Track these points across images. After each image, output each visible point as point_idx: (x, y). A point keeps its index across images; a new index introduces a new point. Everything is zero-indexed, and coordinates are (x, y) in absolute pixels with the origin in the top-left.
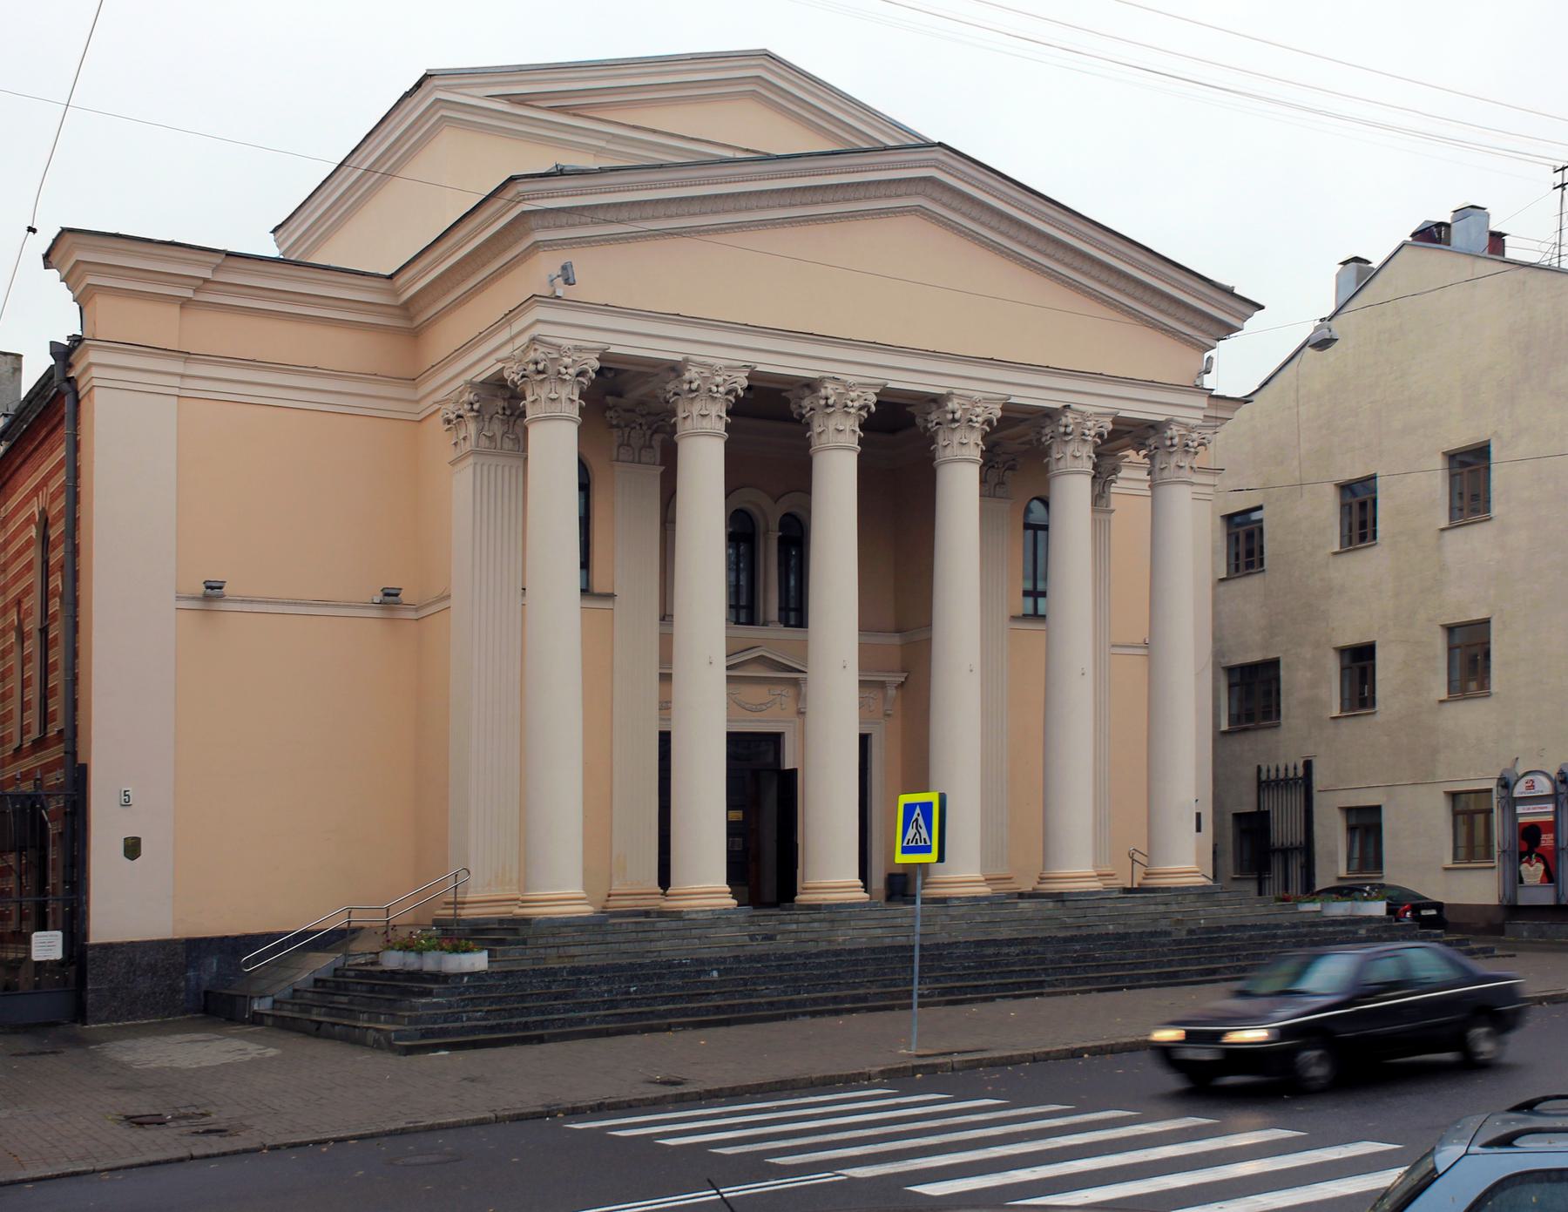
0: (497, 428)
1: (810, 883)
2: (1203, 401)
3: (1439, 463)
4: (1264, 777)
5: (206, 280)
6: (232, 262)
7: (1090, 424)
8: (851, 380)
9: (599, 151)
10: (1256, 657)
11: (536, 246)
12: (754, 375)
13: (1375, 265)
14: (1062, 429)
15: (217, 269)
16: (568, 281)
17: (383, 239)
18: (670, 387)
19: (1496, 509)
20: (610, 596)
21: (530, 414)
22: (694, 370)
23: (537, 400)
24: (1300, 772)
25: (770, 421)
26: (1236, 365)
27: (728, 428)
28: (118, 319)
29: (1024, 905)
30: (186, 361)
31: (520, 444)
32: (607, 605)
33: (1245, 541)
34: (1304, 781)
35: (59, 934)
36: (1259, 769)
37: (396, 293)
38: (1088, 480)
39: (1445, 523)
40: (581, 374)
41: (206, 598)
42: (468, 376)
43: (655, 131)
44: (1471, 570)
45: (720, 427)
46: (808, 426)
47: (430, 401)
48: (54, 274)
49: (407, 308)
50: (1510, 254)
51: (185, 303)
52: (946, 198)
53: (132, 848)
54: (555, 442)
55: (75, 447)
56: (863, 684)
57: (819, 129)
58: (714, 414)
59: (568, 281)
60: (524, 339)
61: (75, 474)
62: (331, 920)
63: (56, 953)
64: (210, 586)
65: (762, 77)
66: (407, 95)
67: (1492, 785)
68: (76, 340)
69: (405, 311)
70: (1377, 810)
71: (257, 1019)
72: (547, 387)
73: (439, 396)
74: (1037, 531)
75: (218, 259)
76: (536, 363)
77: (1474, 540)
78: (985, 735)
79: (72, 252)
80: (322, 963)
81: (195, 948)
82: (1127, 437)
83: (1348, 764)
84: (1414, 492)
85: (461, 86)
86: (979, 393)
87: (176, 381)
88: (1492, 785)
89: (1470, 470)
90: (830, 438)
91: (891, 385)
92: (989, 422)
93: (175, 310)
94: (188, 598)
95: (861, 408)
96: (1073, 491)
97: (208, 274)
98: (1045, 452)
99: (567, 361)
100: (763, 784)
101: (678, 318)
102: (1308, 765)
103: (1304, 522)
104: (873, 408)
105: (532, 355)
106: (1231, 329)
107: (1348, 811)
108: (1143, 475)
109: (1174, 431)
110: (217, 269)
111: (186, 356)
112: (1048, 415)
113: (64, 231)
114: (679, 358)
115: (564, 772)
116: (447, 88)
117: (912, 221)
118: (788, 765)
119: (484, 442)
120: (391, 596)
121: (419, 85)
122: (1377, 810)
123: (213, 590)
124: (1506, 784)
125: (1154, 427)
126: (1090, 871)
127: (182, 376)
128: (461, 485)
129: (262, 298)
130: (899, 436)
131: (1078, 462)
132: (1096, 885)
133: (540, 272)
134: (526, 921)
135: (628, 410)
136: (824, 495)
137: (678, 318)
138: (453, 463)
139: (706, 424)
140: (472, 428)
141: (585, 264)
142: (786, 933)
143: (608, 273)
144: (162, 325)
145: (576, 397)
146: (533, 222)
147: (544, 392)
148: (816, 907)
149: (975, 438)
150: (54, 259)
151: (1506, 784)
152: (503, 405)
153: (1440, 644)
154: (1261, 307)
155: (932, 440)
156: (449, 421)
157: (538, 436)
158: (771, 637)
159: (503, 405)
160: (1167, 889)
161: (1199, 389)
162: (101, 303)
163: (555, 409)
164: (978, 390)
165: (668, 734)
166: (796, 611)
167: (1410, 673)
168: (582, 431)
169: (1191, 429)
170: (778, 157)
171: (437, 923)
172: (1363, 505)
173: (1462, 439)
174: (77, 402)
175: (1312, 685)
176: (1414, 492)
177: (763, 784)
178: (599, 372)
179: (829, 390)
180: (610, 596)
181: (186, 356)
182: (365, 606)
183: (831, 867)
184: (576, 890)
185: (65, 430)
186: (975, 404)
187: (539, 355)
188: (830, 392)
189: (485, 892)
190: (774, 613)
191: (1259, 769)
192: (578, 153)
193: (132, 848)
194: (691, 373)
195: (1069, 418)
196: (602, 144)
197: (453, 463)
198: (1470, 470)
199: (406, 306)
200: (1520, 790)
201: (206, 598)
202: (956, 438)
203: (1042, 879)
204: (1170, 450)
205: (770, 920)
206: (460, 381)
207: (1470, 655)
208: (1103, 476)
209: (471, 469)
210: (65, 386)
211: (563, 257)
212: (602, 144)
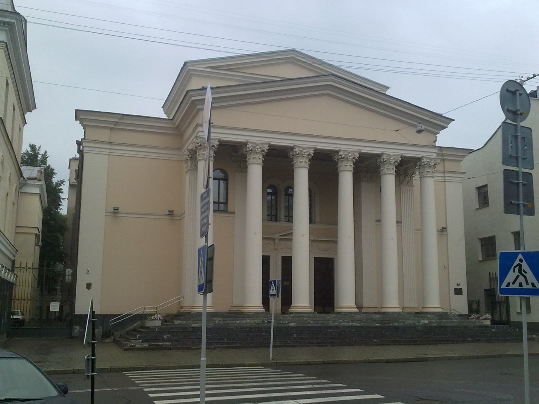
1: (340, 305)
2: (436, 151)
4: (491, 276)
5: (117, 122)
8: (304, 146)
14: (382, 160)
15: (120, 119)
22: (250, 144)
25: (278, 161)
32: (231, 215)
36: (490, 273)
41: (114, 212)
49: (177, 127)
51: (111, 129)
53: (89, 286)
56: (264, 238)
57: (311, 70)
58: (257, 157)
65: (292, 57)
72: (202, 151)
75: (120, 116)
76: (198, 143)
79: (80, 115)
86: (349, 149)
87: (108, 151)
91: (318, 147)
94: (109, 213)
95: (308, 155)
97: (117, 120)
101: (245, 129)
104: (313, 155)
109: (424, 160)
110: (120, 119)
114: (245, 141)
116: (193, 66)
120: (171, 212)
127: (110, 149)
129: (145, 128)
130: (324, 165)
135: (230, 158)
136: (307, 182)
137: (245, 129)
142: (329, 319)
144: (104, 135)
147: (201, 152)
148: (339, 313)
152: (193, 156)
154: (454, 120)
158: (282, 224)
161: (434, 147)
166: (289, 218)
170: (292, 79)
180: (234, 213)
183: (346, 300)
187: (198, 141)
191: (490, 273)
193: (89, 286)
194: (249, 145)
196: (241, 79)
201: (114, 212)
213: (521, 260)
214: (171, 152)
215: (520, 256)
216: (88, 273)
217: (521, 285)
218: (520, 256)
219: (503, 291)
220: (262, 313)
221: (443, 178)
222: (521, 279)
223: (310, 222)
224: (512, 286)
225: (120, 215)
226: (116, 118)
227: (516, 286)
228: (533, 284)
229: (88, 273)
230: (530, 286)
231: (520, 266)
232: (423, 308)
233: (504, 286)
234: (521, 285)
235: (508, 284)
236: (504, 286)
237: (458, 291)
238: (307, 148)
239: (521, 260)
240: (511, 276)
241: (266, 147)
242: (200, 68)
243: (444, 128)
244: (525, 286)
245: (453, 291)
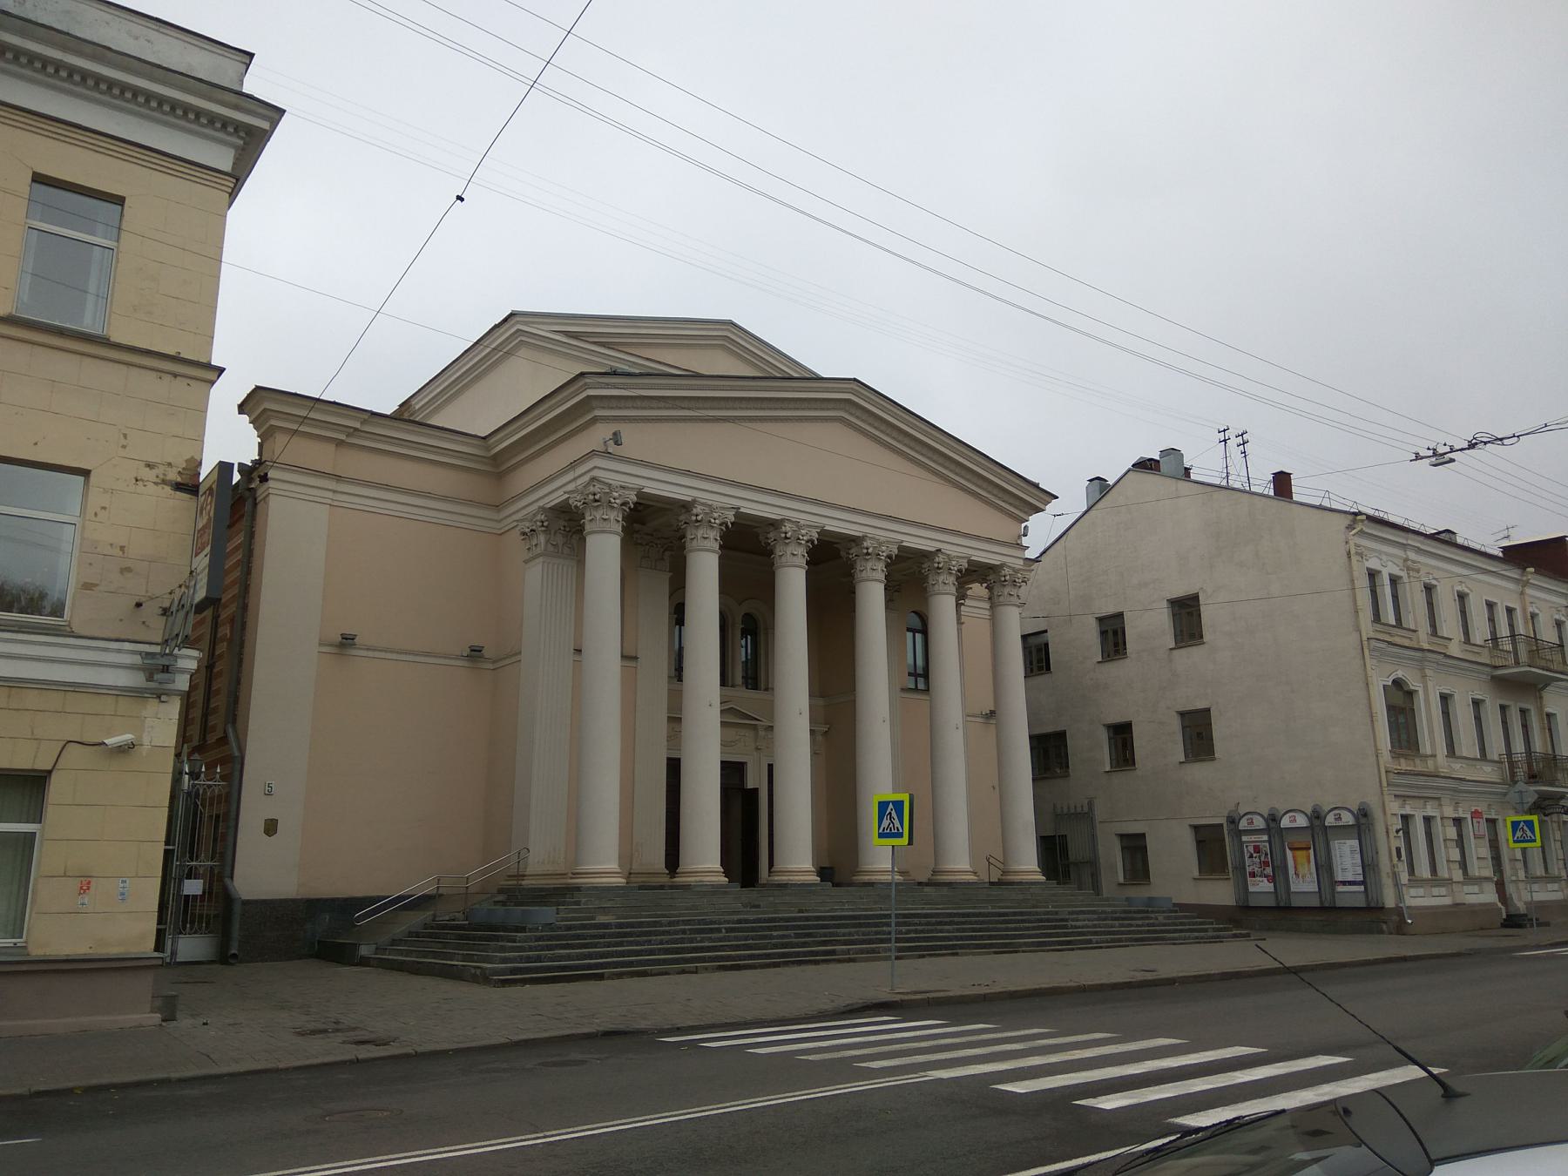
0: (560, 539)
3: (1165, 604)
6: (376, 419)
10: (1049, 729)
11: (595, 420)
12: (739, 514)
13: (1111, 482)
15: (364, 422)
16: (618, 443)
17: (484, 413)
18: (682, 517)
19: (1208, 636)
21: (588, 528)
23: (593, 519)
24: (1086, 809)
25: (749, 546)
26: (1040, 531)
27: (721, 547)
29: (927, 889)
31: (580, 560)
33: (1038, 656)
34: (1085, 816)
37: (488, 449)
38: (882, 586)
39: (1173, 645)
42: (541, 503)
44: (1197, 676)
45: (882, 577)
46: (771, 552)
47: (515, 517)
48: (245, 418)
49: (496, 460)
50: (1193, 477)
52: (859, 413)
53: (271, 827)
54: (605, 549)
55: (251, 535)
59: (618, 443)
60: (586, 478)
61: (249, 554)
62: (420, 886)
64: (344, 637)
65: (727, 335)
66: (496, 326)
67: (1223, 821)
68: (258, 463)
69: (496, 460)
70: (1143, 835)
71: (364, 962)
73: (515, 517)
74: (923, 628)
77: (1191, 656)
78: (894, 768)
80: (416, 919)
81: (313, 907)
82: (976, 573)
83: (1117, 805)
84: (1149, 625)
86: (886, 536)
87: (330, 495)
88: (1223, 821)
89: (1186, 613)
90: (867, 574)
92: (889, 557)
93: (332, 447)
96: (944, 606)
97: (358, 425)
98: (925, 579)
100: (745, 809)
102: (1091, 804)
103: (1077, 643)
105: (591, 489)
107: (1122, 836)
108: (987, 606)
109: (1006, 571)
110: (364, 422)
112: (926, 556)
113: (258, 388)
115: (603, 763)
116: (526, 323)
117: (837, 426)
118: (750, 785)
119: (551, 548)
120: (476, 653)
121: (505, 320)
122: (1143, 835)
123: (347, 641)
124: (1233, 821)
128: (536, 579)
130: (832, 561)
132: (972, 878)
133: (598, 436)
134: (578, 889)
135: (655, 532)
137: (687, 473)
138: (526, 562)
140: (542, 538)
141: (626, 430)
143: (640, 440)
146: (595, 403)
149: (881, 566)
150: (247, 409)
151: (1233, 821)
152: (567, 526)
153: (1176, 725)
155: (852, 566)
156: (524, 534)
157: (592, 541)
159: (567, 526)
160: (1020, 883)
162: (280, 440)
163: (606, 526)
167: (1159, 743)
168: (622, 540)
169: (1016, 571)
171: (501, 891)
172: (1115, 633)
173: (1180, 591)
174: (255, 504)
175: (1089, 749)
176: (1149, 625)
177: (745, 809)
178: (636, 504)
179: (788, 527)
182: (457, 658)
183: (796, 850)
184: (613, 866)
185: (244, 522)
186: (881, 544)
187: (596, 489)
189: (541, 857)
190: (739, 680)
192: (618, 371)
193: (271, 827)
194: (698, 509)
195: (940, 558)
197: (526, 562)
198: (1186, 613)
200: (1243, 824)
202: (869, 565)
203: (935, 872)
204: (1003, 584)
205: (750, 894)
206: (535, 507)
207: (1198, 733)
208: (961, 597)
209: (540, 567)
210: (247, 494)
211: (614, 427)
214: (474, 511)
216: (269, 794)
223: (723, 683)
225: (354, 652)
226: (356, 418)
229: (269, 794)
232: (1005, 873)
241: (730, 517)
243: (1038, 510)
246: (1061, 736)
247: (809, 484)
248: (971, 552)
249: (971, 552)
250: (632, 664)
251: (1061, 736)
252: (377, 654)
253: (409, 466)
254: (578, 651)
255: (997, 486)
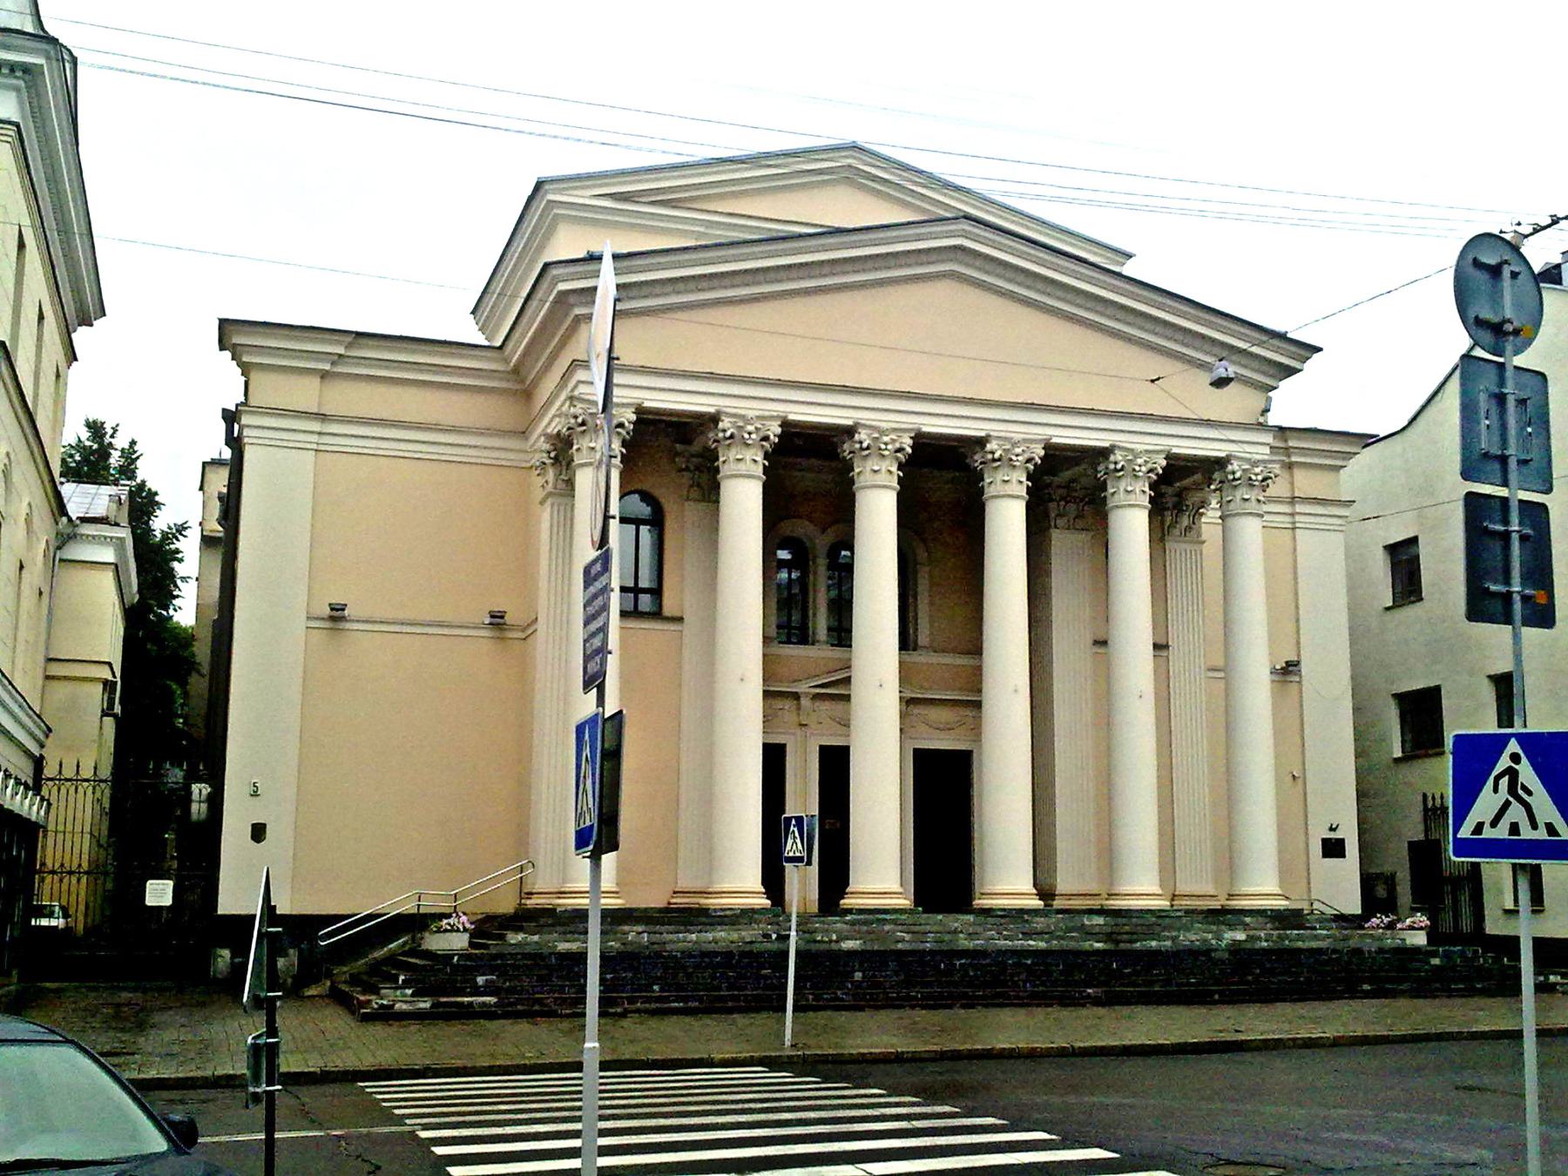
4: (1430, 805)
5: (340, 356)
7: (1140, 461)
8: (884, 425)
9: (684, 233)
14: (1112, 466)
15: (349, 346)
20: (680, 619)
21: (577, 461)
22: (727, 420)
25: (810, 469)
28: (270, 390)
30: (323, 421)
35: (171, 883)
36: (1425, 796)
37: (506, 361)
40: (1029, 460)
41: (332, 618)
43: (750, 217)
45: (759, 470)
51: (324, 375)
53: (258, 832)
63: (167, 901)
65: (851, 165)
72: (587, 438)
75: (349, 339)
76: (576, 417)
85: (576, 188)
87: (315, 438)
93: (316, 381)
97: (341, 351)
99: (750, 428)
104: (909, 450)
106: (1290, 371)
109: (1235, 466)
110: (349, 346)
111: (322, 417)
117: (943, 289)
119: (561, 485)
123: (337, 614)
125: (1221, 463)
126: (1277, 890)
130: (942, 481)
131: (878, 477)
135: (670, 455)
136: (891, 528)
139: (1132, 499)
142: (959, 931)
144: (305, 393)
145: (1024, 479)
152: (562, 451)
154: (1320, 350)
158: (820, 653)
164: (1140, 444)
165: (845, 751)
179: (863, 436)
180: (680, 619)
181: (322, 417)
183: (1006, 877)
186: (1015, 444)
187: (577, 410)
188: (1236, 467)
191: (1425, 796)
192: (737, 238)
193: (258, 832)
196: (702, 229)
199: (516, 371)
201: (332, 618)
212: (702, 229)
213: (1515, 758)
215: (1513, 746)
217: (1514, 829)
218: (1513, 746)
219: (1463, 847)
220: (763, 911)
221: (1288, 519)
222: (1516, 813)
224: (1488, 833)
225: (348, 626)
226: (338, 343)
227: (1501, 832)
228: (1551, 829)
229: (255, 794)
230: (1541, 834)
231: (1512, 774)
233: (1465, 832)
234: (1514, 829)
235: (1479, 828)
236: (1465, 832)
237: (1333, 848)
238: (895, 430)
239: (1515, 758)
240: (1487, 803)
241: (775, 429)
242: (582, 197)
244: (1527, 833)
245: (1317, 848)
246: (264, 826)
247: (899, 368)
248: (1050, 431)
249: (1050, 431)
250: (1101, 650)
251: (264, 826)
252: (377, 627)
253: (366, 389)
254: (1102, 643)
255: (1123, 307)
